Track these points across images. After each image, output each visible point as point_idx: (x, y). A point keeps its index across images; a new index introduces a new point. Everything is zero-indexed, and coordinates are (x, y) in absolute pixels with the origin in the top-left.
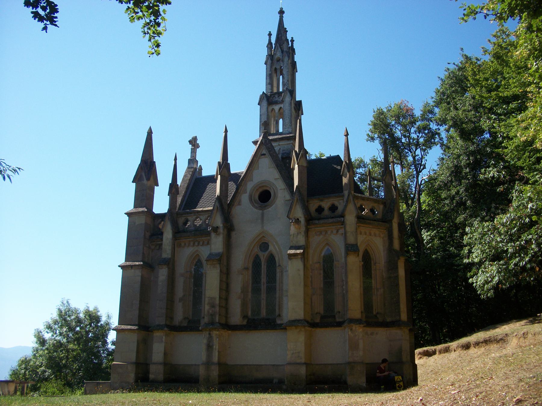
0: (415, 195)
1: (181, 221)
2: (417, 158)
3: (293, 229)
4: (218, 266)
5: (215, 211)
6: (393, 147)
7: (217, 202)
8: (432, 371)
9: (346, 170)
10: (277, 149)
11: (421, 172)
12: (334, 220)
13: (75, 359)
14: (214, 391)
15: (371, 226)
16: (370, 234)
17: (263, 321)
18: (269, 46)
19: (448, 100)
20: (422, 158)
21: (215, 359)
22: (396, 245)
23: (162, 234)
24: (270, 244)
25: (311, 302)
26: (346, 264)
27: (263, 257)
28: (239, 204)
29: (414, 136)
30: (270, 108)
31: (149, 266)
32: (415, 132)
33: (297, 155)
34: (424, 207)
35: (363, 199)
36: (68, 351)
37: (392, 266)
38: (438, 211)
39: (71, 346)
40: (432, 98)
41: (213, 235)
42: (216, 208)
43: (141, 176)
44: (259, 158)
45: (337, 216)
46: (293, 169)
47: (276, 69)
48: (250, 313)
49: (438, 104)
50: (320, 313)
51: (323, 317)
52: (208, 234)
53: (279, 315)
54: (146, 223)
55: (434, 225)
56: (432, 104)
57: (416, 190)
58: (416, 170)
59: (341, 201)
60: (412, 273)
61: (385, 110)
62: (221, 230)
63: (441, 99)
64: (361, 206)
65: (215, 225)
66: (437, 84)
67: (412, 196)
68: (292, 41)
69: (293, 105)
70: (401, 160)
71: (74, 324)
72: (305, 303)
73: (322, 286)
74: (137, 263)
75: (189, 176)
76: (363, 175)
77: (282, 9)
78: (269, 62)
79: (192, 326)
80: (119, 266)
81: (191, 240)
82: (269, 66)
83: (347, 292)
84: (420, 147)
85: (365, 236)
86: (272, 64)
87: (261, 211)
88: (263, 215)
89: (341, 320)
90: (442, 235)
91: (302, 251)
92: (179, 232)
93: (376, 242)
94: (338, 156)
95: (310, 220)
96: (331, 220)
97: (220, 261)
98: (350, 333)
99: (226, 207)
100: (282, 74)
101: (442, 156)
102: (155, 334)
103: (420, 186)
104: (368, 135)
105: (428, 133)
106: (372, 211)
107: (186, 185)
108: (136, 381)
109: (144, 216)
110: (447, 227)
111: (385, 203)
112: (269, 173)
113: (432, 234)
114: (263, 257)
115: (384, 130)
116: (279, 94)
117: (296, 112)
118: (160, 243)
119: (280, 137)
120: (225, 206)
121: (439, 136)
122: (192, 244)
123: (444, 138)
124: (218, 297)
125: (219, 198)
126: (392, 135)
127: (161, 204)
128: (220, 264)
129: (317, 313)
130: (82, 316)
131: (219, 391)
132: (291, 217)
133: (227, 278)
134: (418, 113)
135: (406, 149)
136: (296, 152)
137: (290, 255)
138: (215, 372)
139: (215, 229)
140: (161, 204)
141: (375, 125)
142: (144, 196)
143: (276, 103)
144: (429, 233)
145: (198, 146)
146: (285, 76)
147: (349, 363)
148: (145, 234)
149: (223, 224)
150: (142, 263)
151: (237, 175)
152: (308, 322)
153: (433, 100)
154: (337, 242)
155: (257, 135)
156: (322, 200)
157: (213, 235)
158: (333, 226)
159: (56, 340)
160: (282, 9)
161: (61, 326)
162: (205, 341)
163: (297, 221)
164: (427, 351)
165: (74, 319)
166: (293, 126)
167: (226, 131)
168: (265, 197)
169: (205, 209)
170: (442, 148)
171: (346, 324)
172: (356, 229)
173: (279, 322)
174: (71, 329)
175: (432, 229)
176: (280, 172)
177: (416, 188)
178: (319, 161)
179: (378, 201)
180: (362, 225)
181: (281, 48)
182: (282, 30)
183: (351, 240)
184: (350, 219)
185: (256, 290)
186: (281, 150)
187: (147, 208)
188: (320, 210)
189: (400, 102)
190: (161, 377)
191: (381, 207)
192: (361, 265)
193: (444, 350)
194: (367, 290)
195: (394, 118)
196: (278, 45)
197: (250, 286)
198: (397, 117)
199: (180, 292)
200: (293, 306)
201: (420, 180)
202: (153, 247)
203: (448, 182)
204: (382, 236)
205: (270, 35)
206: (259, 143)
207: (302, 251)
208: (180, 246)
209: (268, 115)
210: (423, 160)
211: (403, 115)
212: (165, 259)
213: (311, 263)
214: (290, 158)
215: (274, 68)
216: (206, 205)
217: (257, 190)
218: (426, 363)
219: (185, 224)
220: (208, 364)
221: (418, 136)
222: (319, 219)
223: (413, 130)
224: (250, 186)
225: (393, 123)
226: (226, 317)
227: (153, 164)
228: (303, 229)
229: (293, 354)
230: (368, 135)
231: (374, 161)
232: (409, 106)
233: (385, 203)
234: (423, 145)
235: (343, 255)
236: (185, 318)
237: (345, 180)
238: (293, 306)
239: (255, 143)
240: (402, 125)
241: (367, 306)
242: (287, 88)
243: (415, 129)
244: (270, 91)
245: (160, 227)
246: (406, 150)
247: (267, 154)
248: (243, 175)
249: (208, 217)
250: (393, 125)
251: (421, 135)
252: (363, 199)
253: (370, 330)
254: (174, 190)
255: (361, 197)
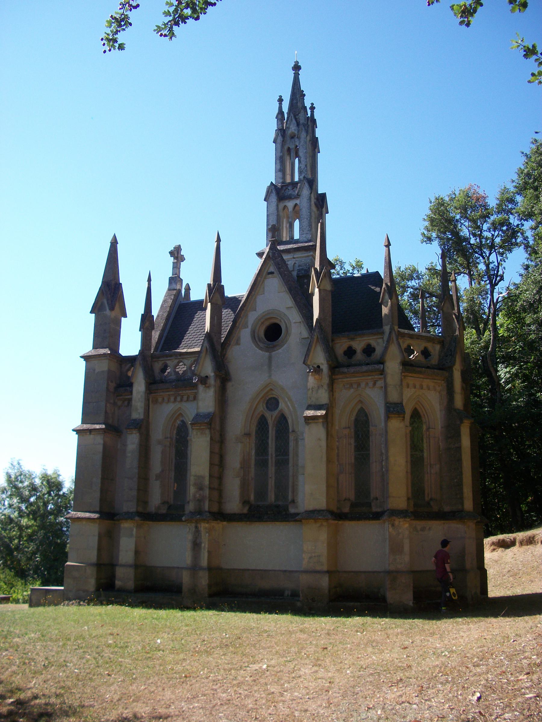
0: (489, 316)
1: (157, 366)
2: (491, 266)
3: (312, 380)
4: (207, 432)
5: (203, 355)
6: (458, 251)
7: (206, 342)
8: (509, 571)
9: (387, 296)
10: (290, 264)
11: (497, 284)
12: (370, 367)
13: (30, 538)
14: (201, 608)
15: (421, 376)
16: (421, 387)
17: (270, 509)
18: (280, 117)
19: (536, 184)
20: (498, 267)
21: (204, 562)
22: (459, 402)
23: (131, 385)
24: (280, 401)
25: (338, 484)
26: (386, 432)
27: (271, 417)
28: (238, 343)
29: (486, 234)
30: (281, 205)
31: (114, 429)
32: (489, 230)
33: (318, 274)
34: (501, 332)
35: (411, 337)
36: (21, 528)
37: (452, 432)
38: (521, 337)
39: (24, 521)
40: (513, 181)
41: (201, 388)
42: (204, 349)
43: (102, 304)
44: (265, 278)
45: (373, 361)
46: (313, 294)
47: (289, 150)
48: (252, 497)
49: (521, 189)
50: (349, 500)
51: (353, 505)
52: (195, 386)
53: (293, 501)
54: (109, 371)
55: (514, 358)
56: (512, 189)
57: (489, 311)
58: (491, 283)
59: (380, 341)
60: (483, 427)
61: (447, 199)
62: (212, 381)
63: (526, 183)
64: (409, 346)
65: (203, 375)
66: (520, 162)
67: (485, 317)
68: (312, 108)
69: (313, 200)
70: (469, 269)
71: (27, 493)
72: (328, 486)
73: (353, 461)
74: (98, 426)
75: (170, 302)
76: (416, 289)
77: (297, 62)
78: (280, 139)
79: (172, 513)
80: (74, 430)
81: (172, 393)
82: (279, 146)
83: (387, 471)
84: (495, 250)
85: (413, 390)
86: (284, 142)
87: (267, 354)
88: (270, 359)
89: (379, 510)
90: (527, 372)
91: (324, 412)
92: (154, 383)
93: (429, 397)
94: (377, 272)
95: (335, 367)
96: (365, 368)
97: (211, 424)
98: (391, 529)
99: (219, 348)
100: (297, 156)
101: (526, 263)
102: (122, 525)
103: (495, 305)
104: (423, 234)
105: (507, 230)
106: (425, 353)
107: (165, 315)
108: (97, 590)
109: (107, 361)
110: (533, 362)
111: (443, 342)
112: (277, 300)
113: (513, 370)
114: (271, 417)
115: (446, 227)
116: (294, 184)
117: (318, 210)
118: (129, 397)
119: (295, 246)
120: (217, 347)
121: (522, 234)
122: (172, 399)
123: (529, 236)
124: (207, 474)
125: (208, 336)
126: (456, 234)
127: (130, 343)
128: (210, 429)
129: (345, 500)
130: (38, 482)
131: (209, 608)
132: (309, 363)
133: (221, 448)
134: (492, 202)
135: (476, 253)
136: (316, 269)
137: (308, 419)
138: (204, 580)
139: (204, 380)
140: (130, 343)
141: (432, 220)
142: (107, 331)
143: (290, 198)
144: (508, 369)
145: (183, 259)
146: (302, 159)
147: (389, 572)
148: (108, 385)
149: (215, 372)
150: (104, 426)
151: (235, 300)
152: (332, 513)
153: (514, 184)
154: (374, 399)
155: (263, 245)
156: (353, 339)
157: (201, 388)
158: (369, 376)
159: (5, 515)
160: (297, 62)
161: (11, 495)
162: (190, 537)
163: (318, 370)
164: (503, 540)
165: (28, 486)
166: (313, 230)
167: (219, 240)
168: (273, 333)
169: (190, 350)
170: (527, 251)
171: (385, 517)
172: (402, 381)
173: (292, 510)
174: (24, 500)
175: (512, 363)
176: (295, 300)
177: (489, 308)
178: (348, 282)
179: (432, 339)
180: (410, 375)
181: (296, 119)
182: (297, 93)
183: (394, 397)
184: (393, 366)
185: (262, 463)
186: (297, 265)
187: (110, 350)
188: (350, 352)
189: (467, 187)
190: (130, 585)
191: (438, 347)
192: (408, 432)
193: (527, 541)
194: (416, 462)
195: (459, 211)
196: (292, 115)
197: (253, 458)
198: (464, 209)
199: (156, 465)
200: (311, 489)
201: (496, 296)
202: (120, 403)
203: (534, 301)
204: (438, 389)
205: (281, 100)
206: (264, 257)
207: (324, 412)
208: (156, 402)
209: (278, 215)
210: (500, 268)
211: (472, 206)
212: (135, 420)
213: (337, 428)
214: (309, 277)
215: (286, 148)
216: (192, 344)
217: (262, 323)
218: (502, 558)
219: (164, 370)
220: (194, 568)
221: (493, 235)
222: (349, 366)
223: (485, 226)
224: (252, 317)
225: (458, 217)
226: (220, 503)
227: (118, 287)
228: (326, 380)
229: (310, 558)
230: (423, 234)
231: (432, 270)
232: (481, 193)
233: (443, 342)
234: (501, 247)
235: (383, 418)
236: (164, 503)
237: (385, 310)
238: (311, 489)
239: (260, 255)
240: (470, 220)
241: (417, 490)
242: (304, 177)
243: (488, 225)
244: (281, 181)
245: (130, 374)
246: (477, 255)
247: (276, 273)
248: (244, 298)
249: (194, 361)
250: (457, 221)
251: (497, 233)
252: (411, 337)
253: (419, 524)
254: (147, 324)
255: (409, 334)
